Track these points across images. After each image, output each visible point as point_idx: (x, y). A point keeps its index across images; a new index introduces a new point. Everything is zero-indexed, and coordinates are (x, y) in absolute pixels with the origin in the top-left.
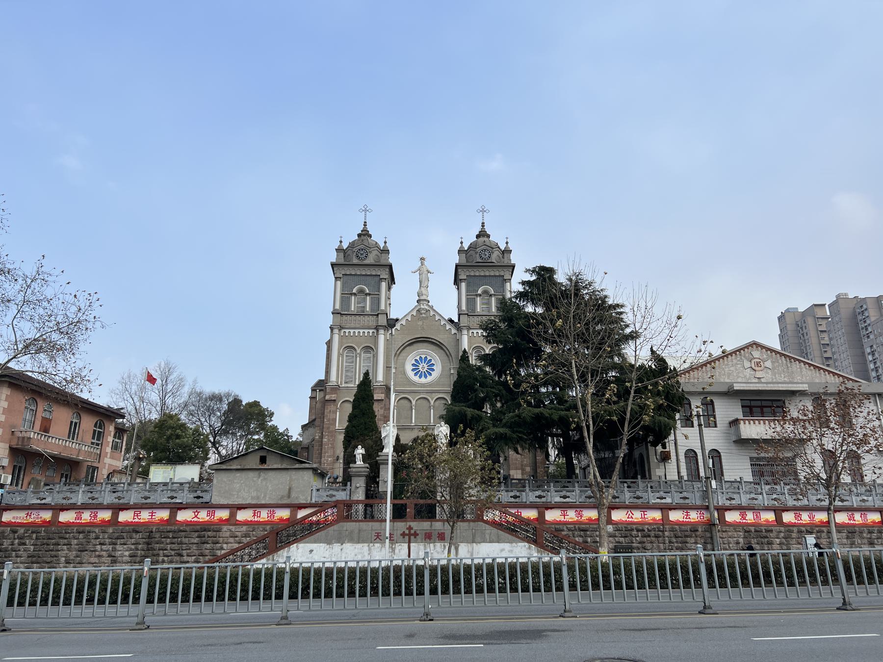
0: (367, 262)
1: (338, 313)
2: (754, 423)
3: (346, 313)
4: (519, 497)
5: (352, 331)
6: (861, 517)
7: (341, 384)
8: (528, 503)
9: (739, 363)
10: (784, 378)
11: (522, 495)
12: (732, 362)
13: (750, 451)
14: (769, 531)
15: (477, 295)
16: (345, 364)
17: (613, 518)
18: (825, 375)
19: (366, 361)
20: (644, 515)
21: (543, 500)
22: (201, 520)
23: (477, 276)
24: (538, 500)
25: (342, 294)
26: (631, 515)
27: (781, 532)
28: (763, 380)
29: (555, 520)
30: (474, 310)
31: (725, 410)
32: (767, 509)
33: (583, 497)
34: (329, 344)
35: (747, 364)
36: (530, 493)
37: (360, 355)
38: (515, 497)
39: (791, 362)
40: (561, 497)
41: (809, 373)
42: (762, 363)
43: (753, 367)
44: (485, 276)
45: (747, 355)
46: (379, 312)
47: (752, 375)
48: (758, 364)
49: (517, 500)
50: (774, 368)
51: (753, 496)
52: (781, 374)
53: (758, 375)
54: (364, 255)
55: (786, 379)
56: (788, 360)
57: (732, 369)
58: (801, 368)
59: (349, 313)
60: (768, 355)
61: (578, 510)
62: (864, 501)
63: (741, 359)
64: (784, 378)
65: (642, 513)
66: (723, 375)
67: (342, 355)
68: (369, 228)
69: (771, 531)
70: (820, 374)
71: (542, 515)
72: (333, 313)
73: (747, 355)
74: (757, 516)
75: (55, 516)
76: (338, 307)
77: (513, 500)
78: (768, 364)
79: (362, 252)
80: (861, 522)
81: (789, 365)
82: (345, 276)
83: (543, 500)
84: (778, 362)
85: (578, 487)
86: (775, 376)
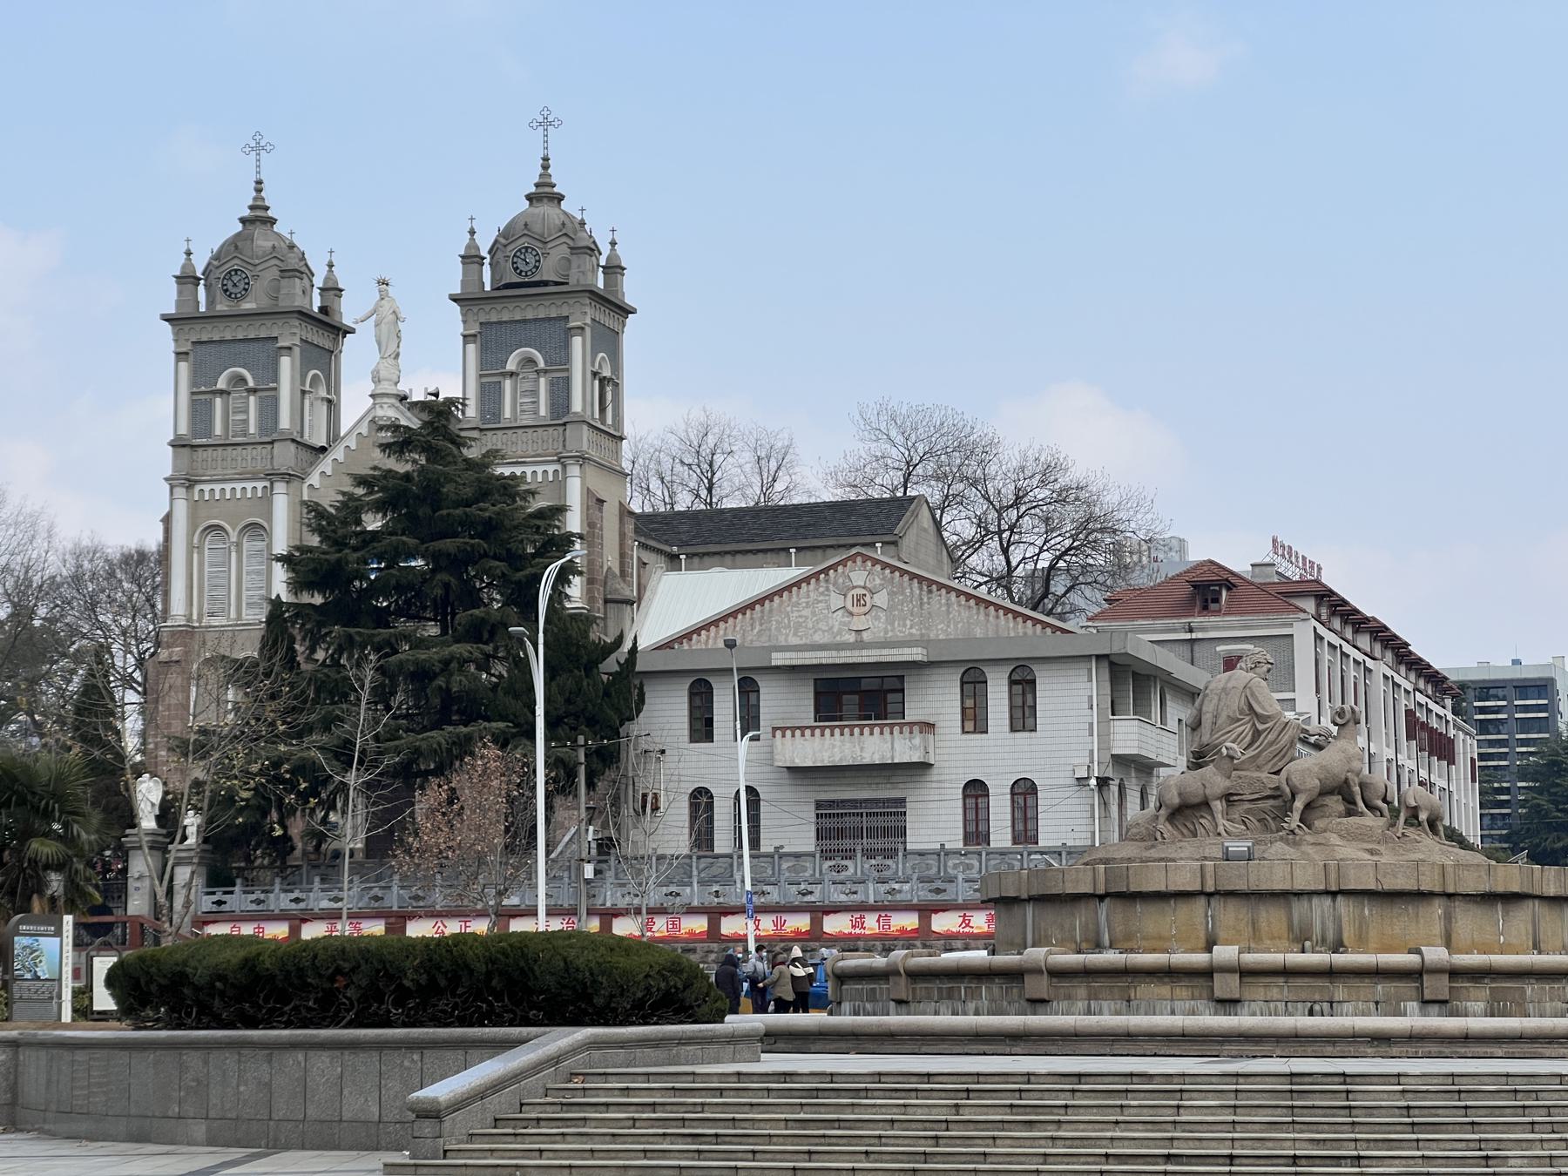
0: (248, 305)
1: (184, 446)
2: (803, 735)
3: (204, 441)
4: (263, 901)
5: (217, 487)
6: (878, 921)
7: (200, 620)
8: (277, 912)
9: (821, 598)
10: (911, 628)
11: (308, 897)
12: (808, 597)
13: (818, 788)
14: (689, 950)
15: (504, 375)
16: (207, 569)
17: (827, 929)
18: (998, 617)
19: (253, 560)
20: (466, 927)
21: (302, 905)
22: (976, 931)
23: (505, 322)
24: (294, 906)
25: (193, 393)
26: (442, 927)
27: (712, 952)
28: (866, 636)
29: (841, 932)
30: (497, 414)
31: (784, 703)
32: (692, 911)
33: (366, 899)
34: (167, 520)
35: (836, 601)
36: (282, 895)
37: (239, 545)
38: (259, 902)
39: (930, 592)
40: (330, 900)
41: (965, 614)
42: (867, 599)
43: (849, 606)
44: (525, 321)
45: (841, 580)
46: (275, 437)
47: (845, 624)
48: (859, 600)
49: (260, 907)
50: (891, 608)
51: (673, 888)
52: (905, 619)
53: (858, 623)
54: (242, 285)
55: (914, 631)
56: (925, 587)
57: (806, 612)
58: (948, 605)
59: (211, 441)
60: (883, 579)
61: (355, 921)
62: (892, 892)
63: (828, 589)
64: (911, 628)
65: (463, 924)
66: (785, 629)
67: (200, 548)
68: (269, 197)
69: (694, 951)
70: (987, 615)
71: (714, 926)
72: (174, 445)
73: (841, 580)
74: (673, 924)
75: (295, 931)
76: (183, 429)
77: (254, 907)
78: (881, 599)
79: (236, 279)
80: (877, 931)
81: (925, 600)
82: (198, 347)
83: (302, 905)
84: (903, 593)
85: (242, 885)
86: (892, 624)
